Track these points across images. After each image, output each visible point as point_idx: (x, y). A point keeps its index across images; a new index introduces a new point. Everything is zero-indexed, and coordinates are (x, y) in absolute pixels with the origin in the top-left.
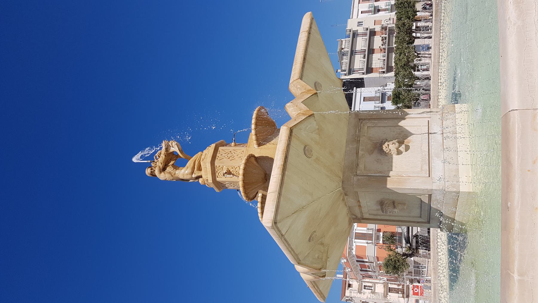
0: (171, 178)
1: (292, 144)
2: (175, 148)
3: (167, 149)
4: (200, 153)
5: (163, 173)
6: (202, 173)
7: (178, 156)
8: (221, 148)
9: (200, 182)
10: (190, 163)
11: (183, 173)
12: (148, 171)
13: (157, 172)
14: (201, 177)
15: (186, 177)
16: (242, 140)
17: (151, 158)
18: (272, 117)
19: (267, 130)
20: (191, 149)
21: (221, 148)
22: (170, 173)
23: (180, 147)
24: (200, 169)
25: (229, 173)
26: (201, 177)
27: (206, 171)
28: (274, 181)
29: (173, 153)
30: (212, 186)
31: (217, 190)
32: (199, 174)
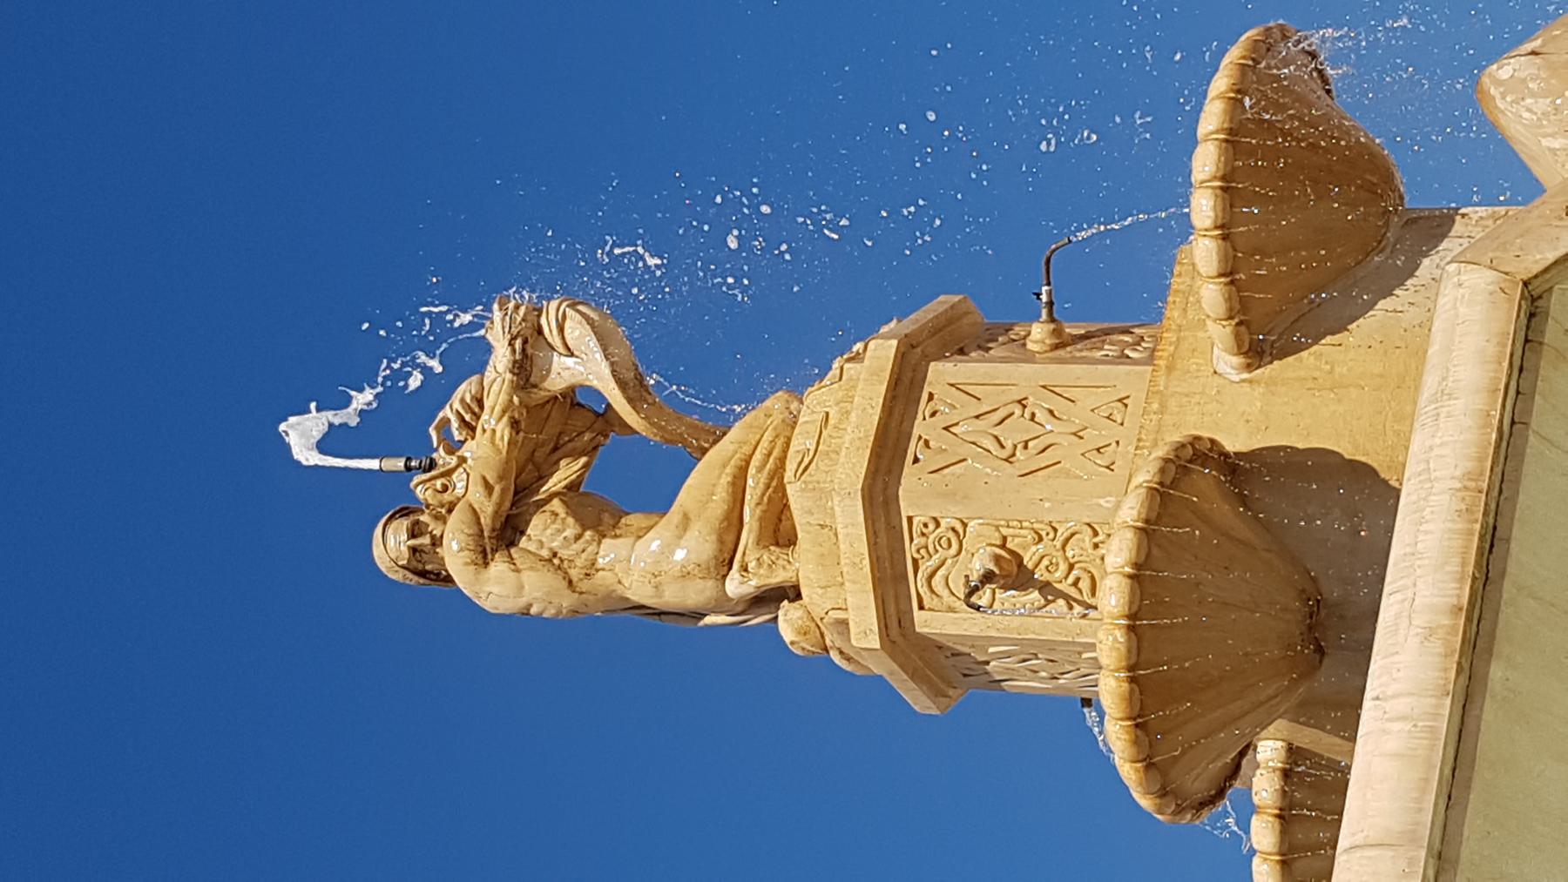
0: (567, 601)
1: (1542, 415)
2: (582, 361)
3: (525, 371)
4: (776, 403)
5: (498, 566)
6: (801, 566)
7: (606, 418)
8: (940, 374)
9: (787, 633)
10: (704, 486)
11: (653, 561)
12: (390, 546)
13: (454, 555)
14: (792, 593)
15: (674, 596)
16: (1112, 306)
17: (405, 426)
18: (1364, 111)
19: (1329, 225)
20: (717, 358)
21: (940, 374)
22: (553, 561)
23: (623, 351)
24: (779, 532)
25: (1011, 573)
26: (792, 593)
27: (830, 558)
28: (1391, 745)
29: (575, 400)
30: (882, 667)
31: (919, 701)
32: (779, 577)
